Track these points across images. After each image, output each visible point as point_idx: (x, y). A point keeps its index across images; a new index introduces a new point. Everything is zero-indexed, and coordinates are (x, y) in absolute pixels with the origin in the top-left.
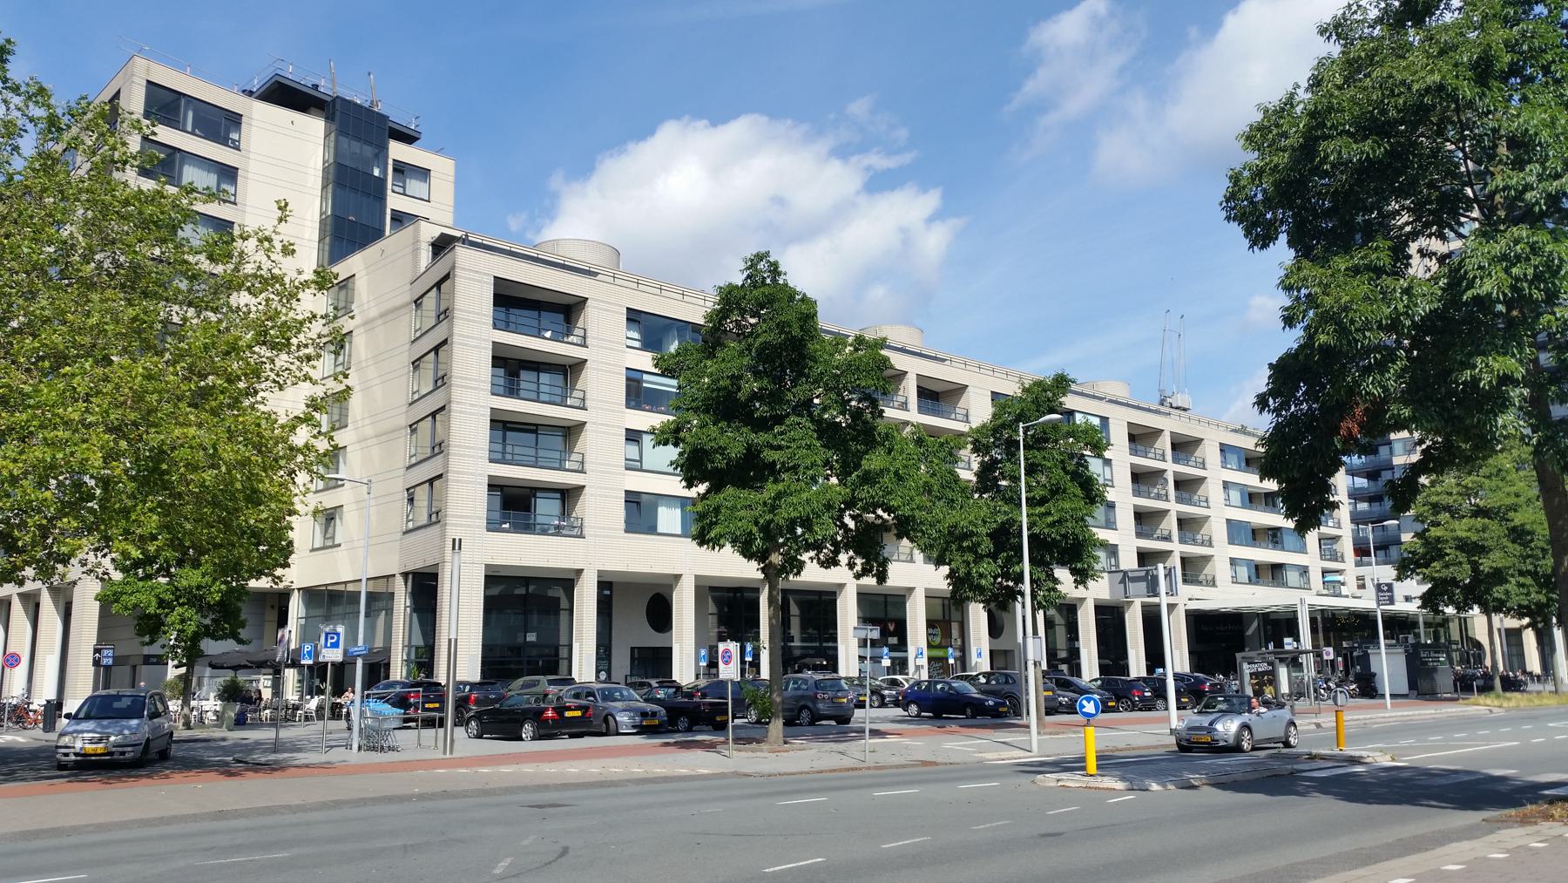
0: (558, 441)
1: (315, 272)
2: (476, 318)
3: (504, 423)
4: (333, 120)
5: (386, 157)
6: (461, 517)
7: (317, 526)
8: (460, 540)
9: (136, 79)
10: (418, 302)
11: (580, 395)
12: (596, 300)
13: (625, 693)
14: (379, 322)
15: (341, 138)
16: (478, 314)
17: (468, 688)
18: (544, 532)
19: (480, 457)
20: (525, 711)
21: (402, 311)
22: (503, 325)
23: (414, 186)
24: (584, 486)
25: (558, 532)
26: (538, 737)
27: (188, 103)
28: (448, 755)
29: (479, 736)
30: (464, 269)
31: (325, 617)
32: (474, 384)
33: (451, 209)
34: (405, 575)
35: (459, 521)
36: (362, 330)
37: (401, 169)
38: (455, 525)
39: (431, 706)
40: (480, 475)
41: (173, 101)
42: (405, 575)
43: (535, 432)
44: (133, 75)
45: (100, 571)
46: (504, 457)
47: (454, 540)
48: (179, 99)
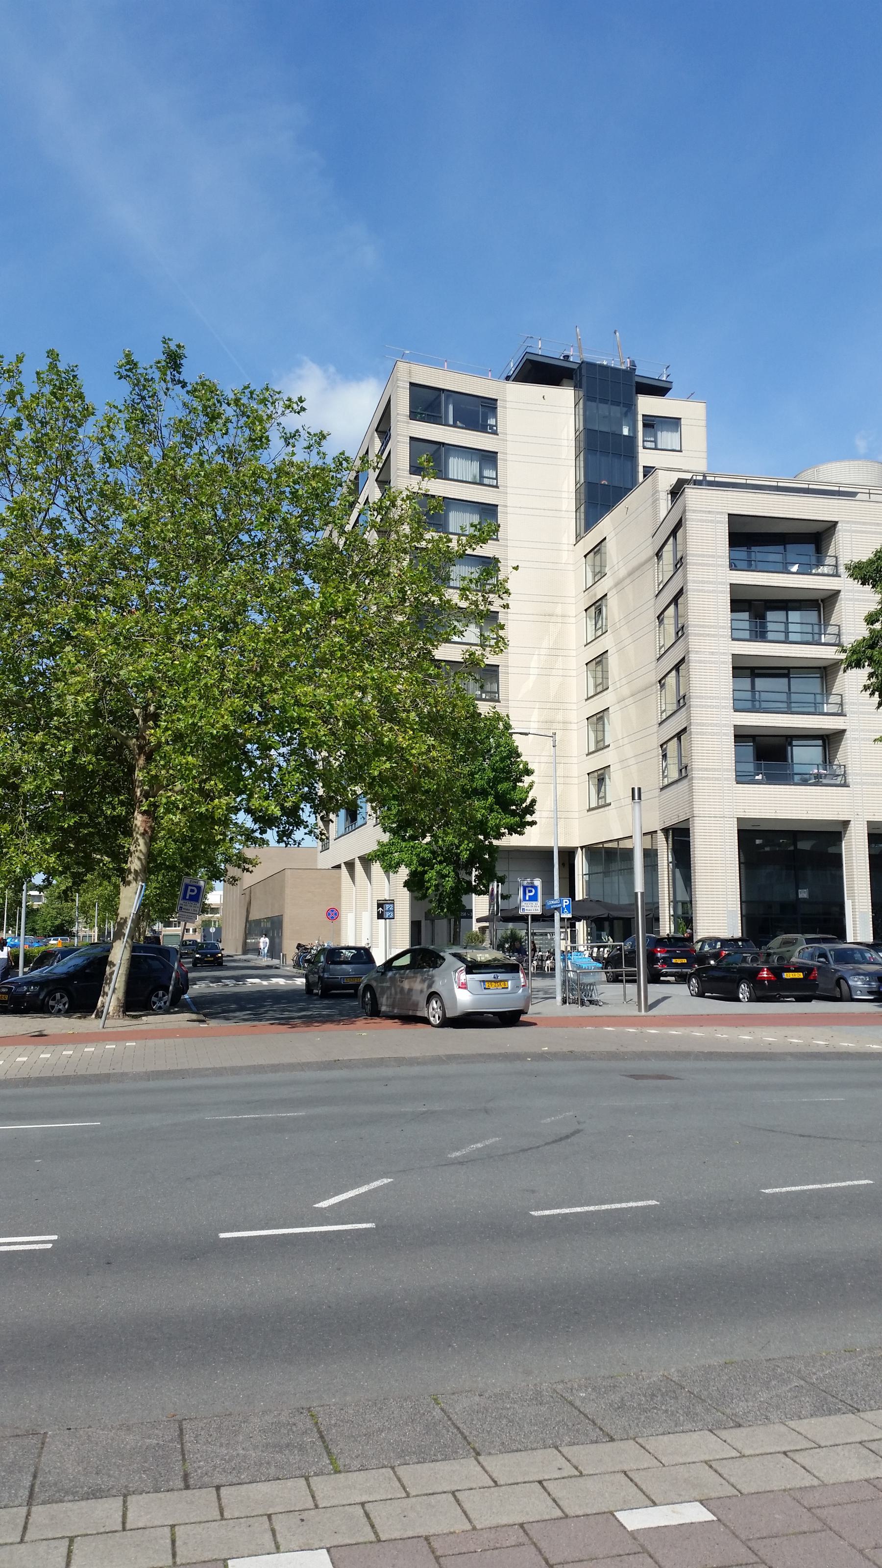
0: (814, 684)
1: (863, 584)
2: (711, 561)
3: (753, 669)
4: (581, 387)
5: (635, 414)
6: (706, 770)
7: (591, 786)
8: (639, 789)
9: (400, 384)
10: (658, 555)
11: (834, 630)
12: (848, 522)
13: (868, 955)
14: (628, 581)
15: (589, 403)
16: (713, 556)
17: (719, 945)
18: (805, 782)
19: (724, 707)
20: (741, 970)
21: (648, 566)
22: (744, 564)
23: (666, 438)
24: (844, 731)
25: (818, 780)
26: (755, 998)
27: (447, 398)
28: (643, 1013)
29: (700, 994)
30: (694, 511)
31: (604, 873)
32: (713, 631)
33: (704, 455)
34: (665, 831)
35: (706, 774)
36: (614, 591)
37: (651, 423)
38: (701, 778)
39: (679, 961)
40: (725, 725)
41: (435, 400)
42: (665, 831)
43: (787, 676)
44: (397, 380)
45: (318, 831)
46: (754, 706)
47: (633, 789)
48: (440, 396)
